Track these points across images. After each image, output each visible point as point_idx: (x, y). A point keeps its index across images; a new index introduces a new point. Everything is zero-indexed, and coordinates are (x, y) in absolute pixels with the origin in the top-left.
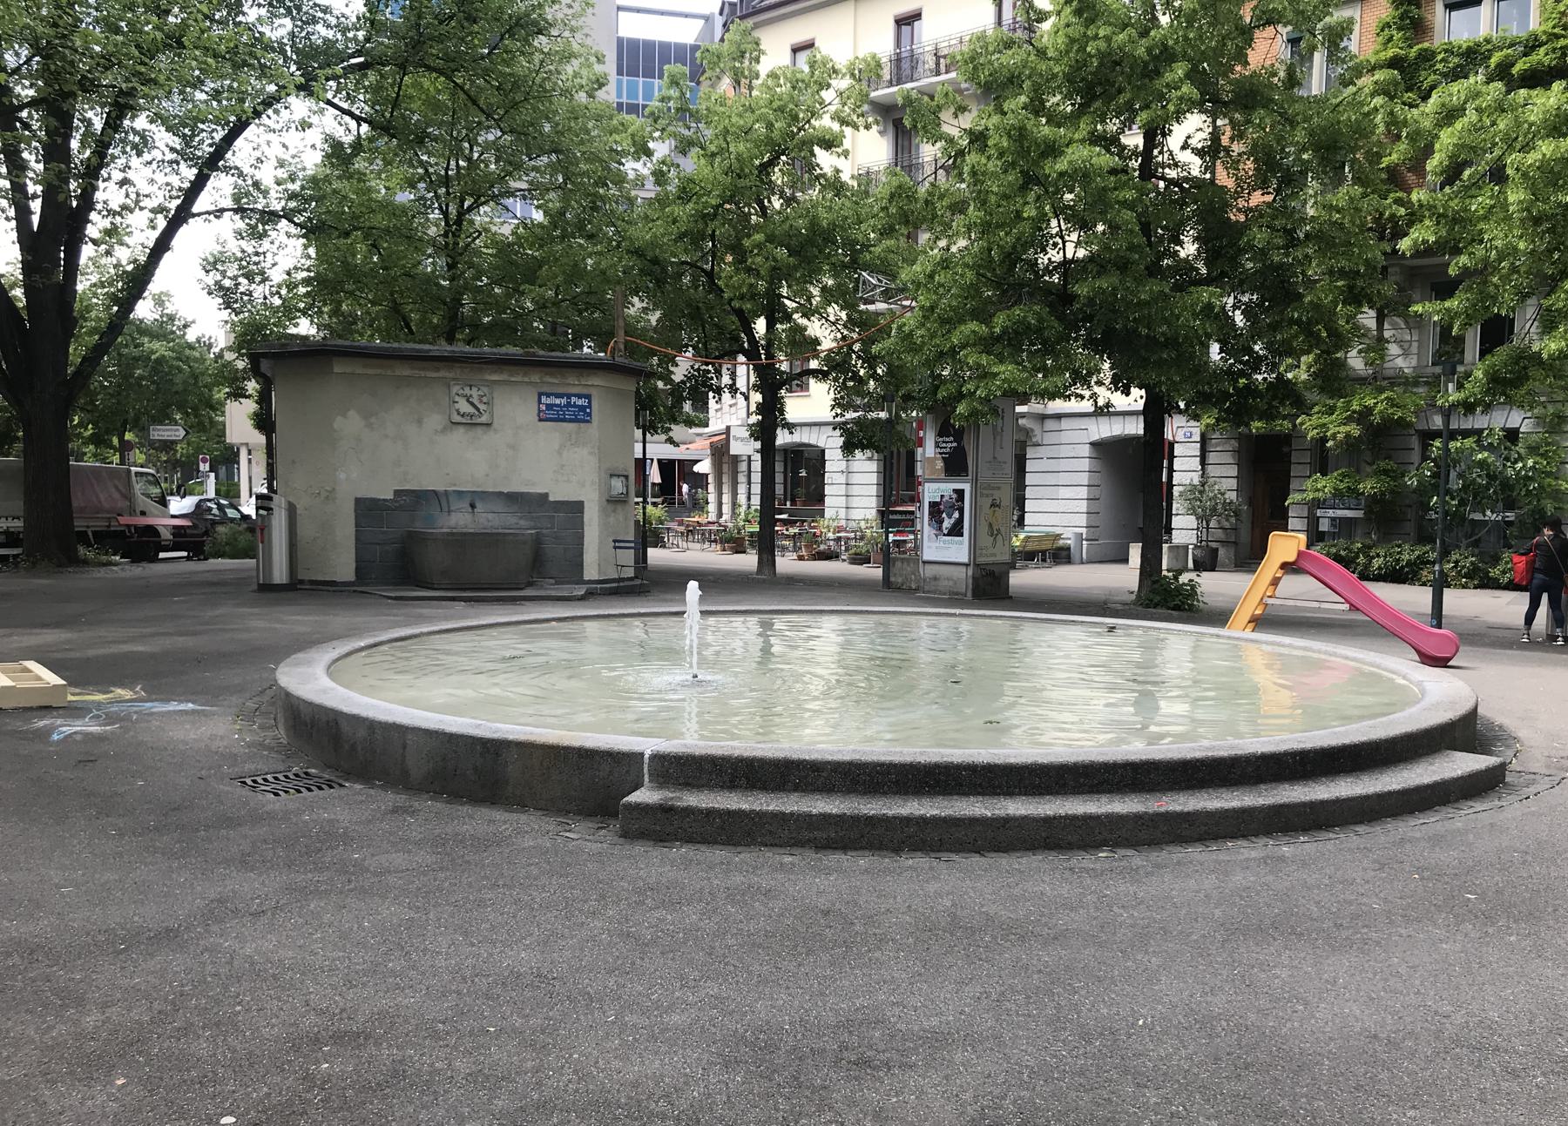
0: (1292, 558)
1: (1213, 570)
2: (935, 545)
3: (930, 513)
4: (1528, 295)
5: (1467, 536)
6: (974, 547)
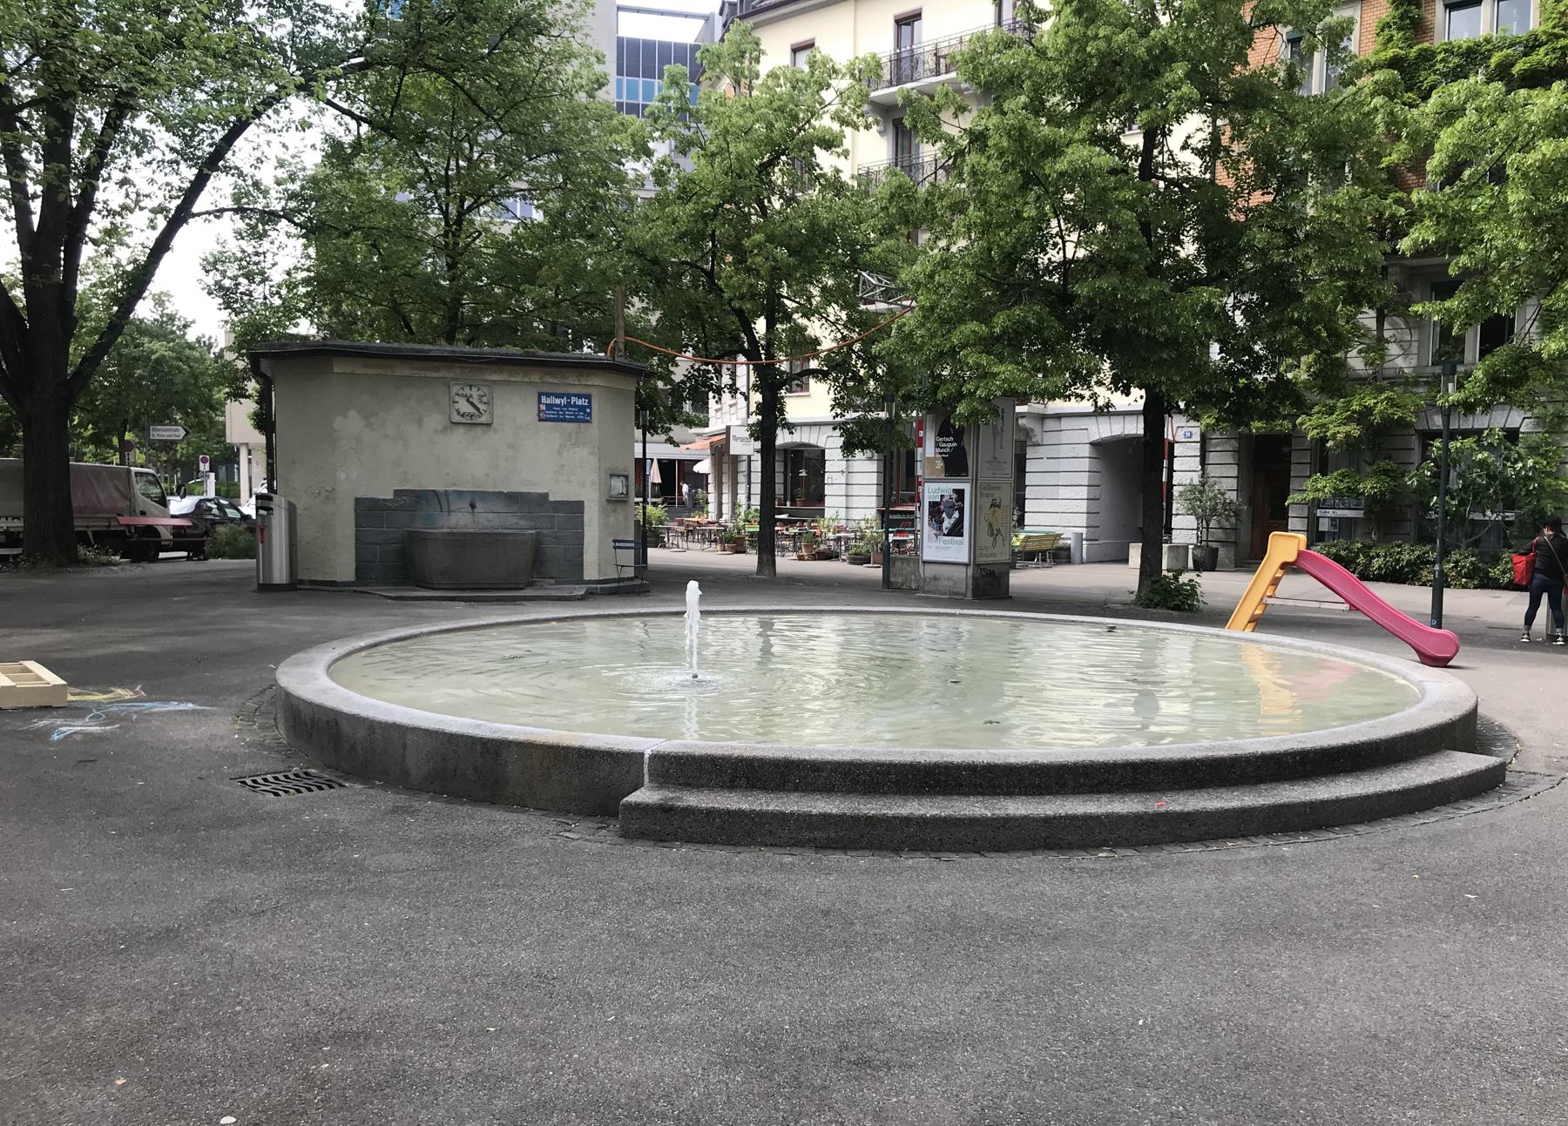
0: (1292, 558)
1: (1213, 570)
2: (935, 545)
3: (930, 513)
4: (1528, 295)
5: (1467, 536)
6: (974, 547)
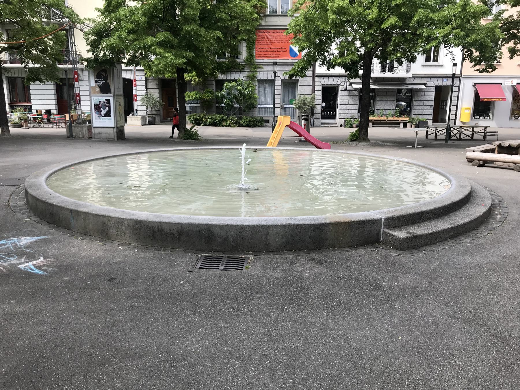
0: (289, 124)
1: (155, 124)
2: (98, 120)
3: (95, 108)
4: (131, 33)
5: (233, 112)
6: (116, 121)
